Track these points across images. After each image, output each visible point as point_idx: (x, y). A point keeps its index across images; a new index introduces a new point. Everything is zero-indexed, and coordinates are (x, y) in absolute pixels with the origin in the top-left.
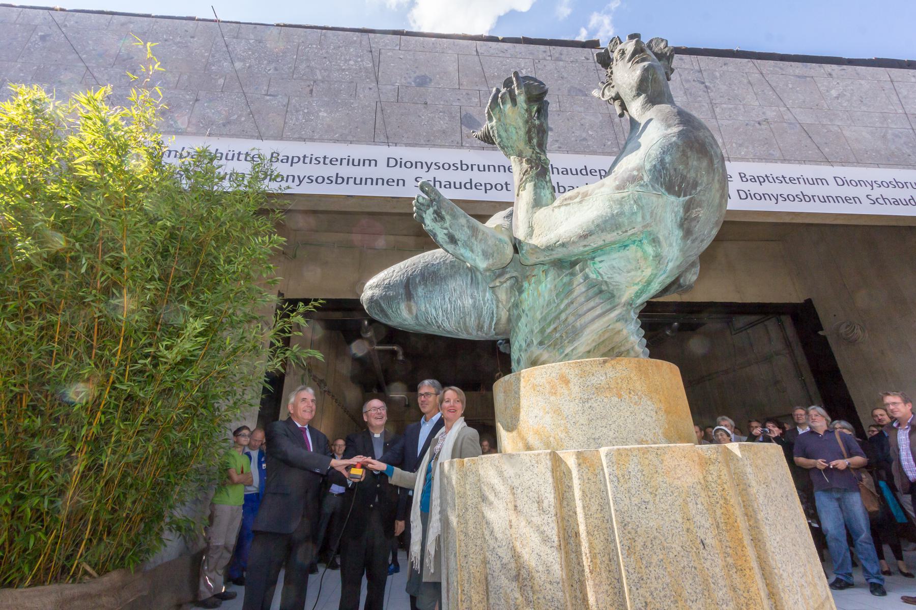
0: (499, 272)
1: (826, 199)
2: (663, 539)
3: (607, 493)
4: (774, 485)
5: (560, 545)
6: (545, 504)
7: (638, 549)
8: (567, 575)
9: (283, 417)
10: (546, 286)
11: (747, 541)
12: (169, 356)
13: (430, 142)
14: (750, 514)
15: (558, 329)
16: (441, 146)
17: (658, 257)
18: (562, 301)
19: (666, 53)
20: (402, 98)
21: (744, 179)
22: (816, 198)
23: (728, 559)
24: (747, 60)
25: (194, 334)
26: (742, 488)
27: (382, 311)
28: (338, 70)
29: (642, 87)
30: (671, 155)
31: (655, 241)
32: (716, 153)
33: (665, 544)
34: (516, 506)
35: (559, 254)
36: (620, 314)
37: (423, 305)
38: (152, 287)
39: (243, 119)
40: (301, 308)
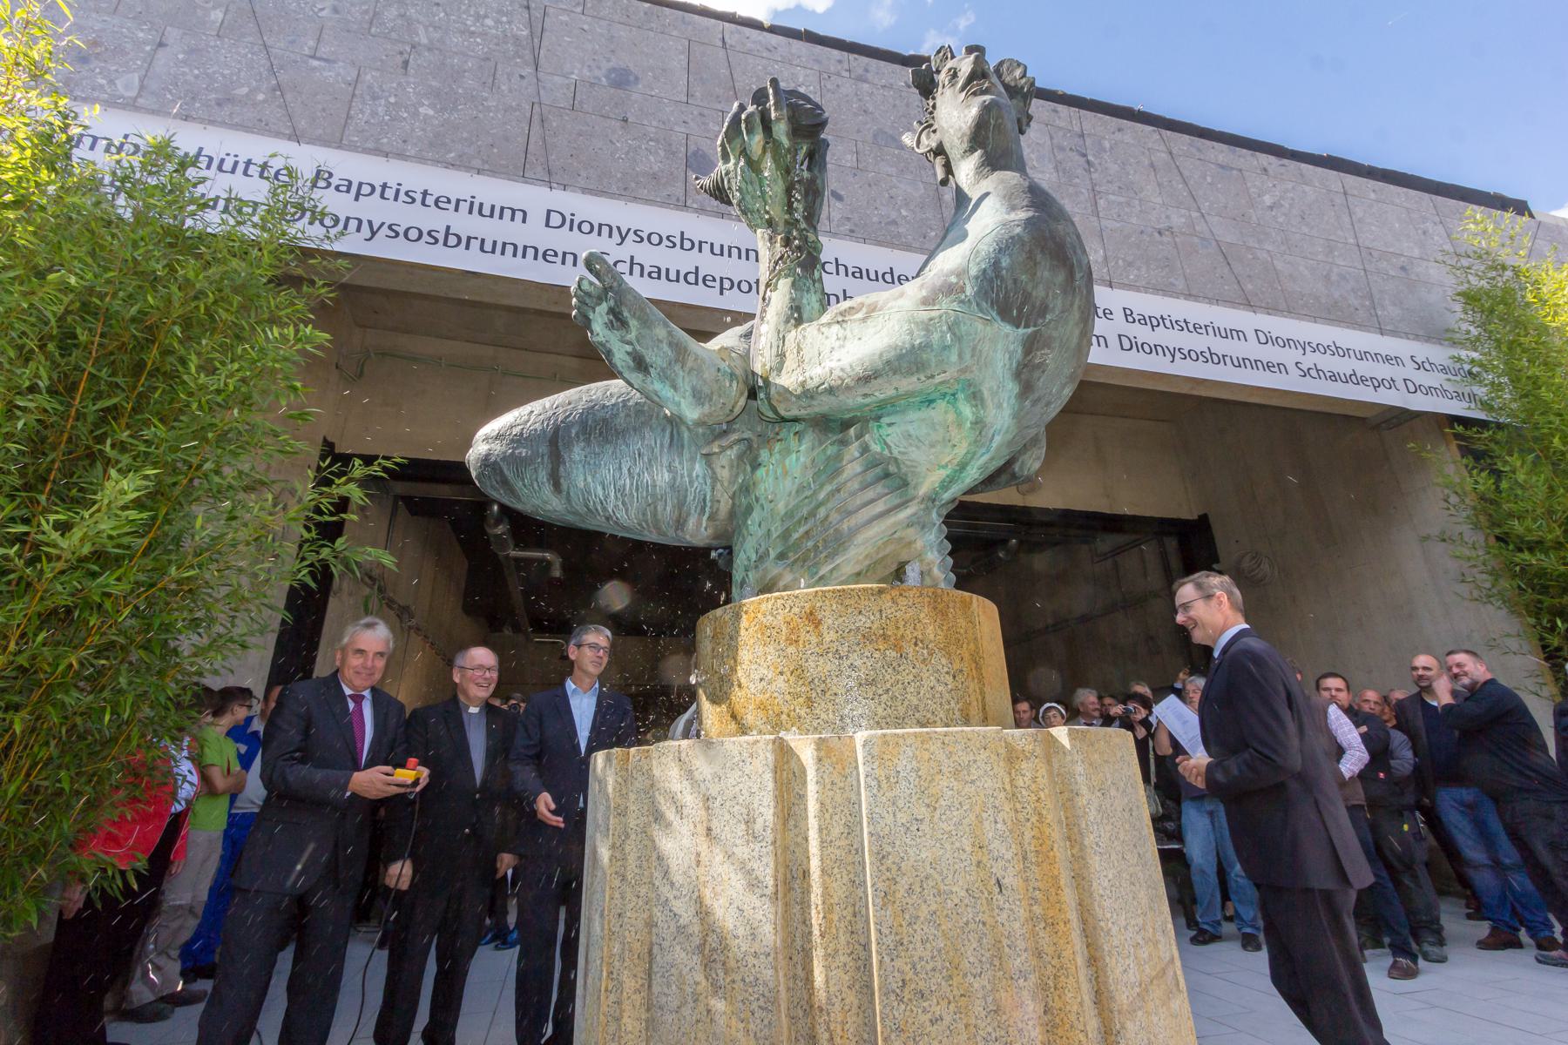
0: (718, 431)
1: (1241, 363)
2: (939, 879)
3: (860, 806)
4: (1113, 792)
5: (776, 893)
6: (758, 826)
7: (898, 895)
8: (784, 941)
9: (321, 670)
10: (798, 459)
11: (1065, 879)
12: (64, 543)
13: (627, 192)
14: (1074, 836)
15: (811, 533)
16: (648, 202)
17: (979, 424)
18: (822, 486)
19: (1022, 88)
20: (581, 102)
21: (1130, 319)
22: (1228, 359)
23: (1035, 908)
24: (1151, 128)
25: (121, 503)
26: (1066, 794)
27: (505, 482)
28: (462, 32)
29: (980, 136)
30: (1010, 255)
31: (976, 397)
32: (1079, 262)
33: (942, 887)
34: (709, 829)
35: (823, 405)
36: (915, 514)
37: (581, 478)
38: (31, 405)
39: (261, 97)
40: (358, 468)
